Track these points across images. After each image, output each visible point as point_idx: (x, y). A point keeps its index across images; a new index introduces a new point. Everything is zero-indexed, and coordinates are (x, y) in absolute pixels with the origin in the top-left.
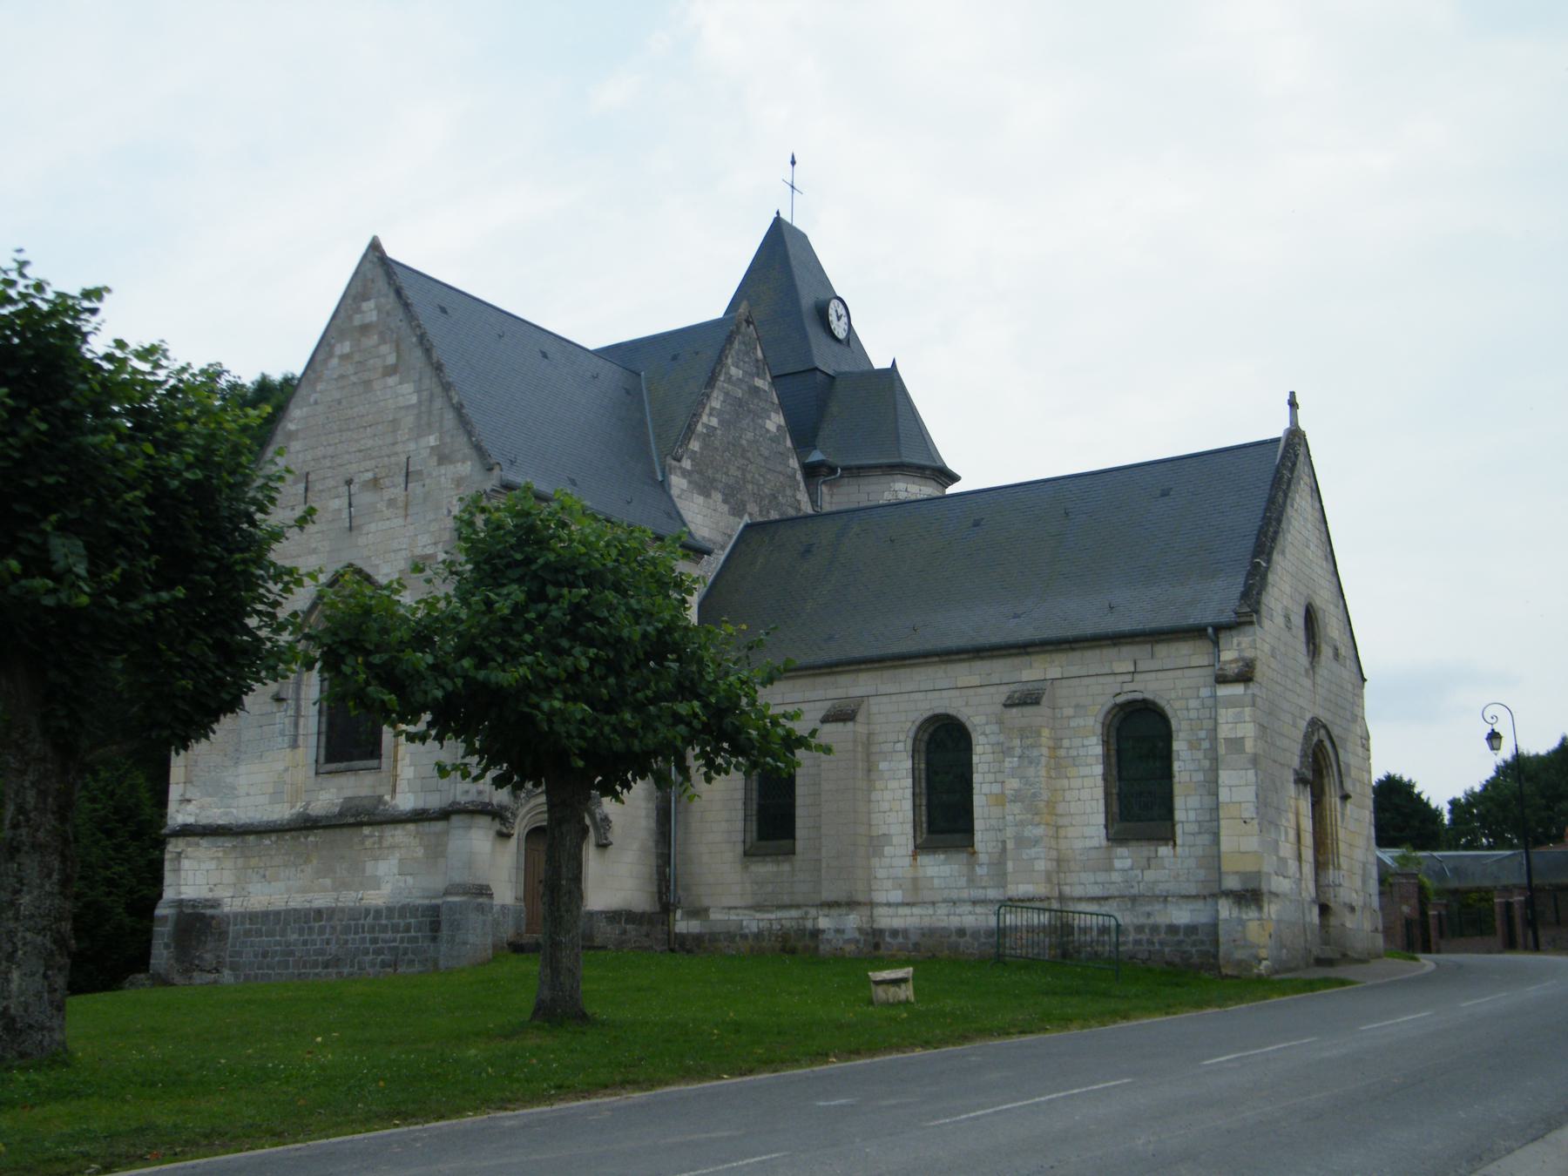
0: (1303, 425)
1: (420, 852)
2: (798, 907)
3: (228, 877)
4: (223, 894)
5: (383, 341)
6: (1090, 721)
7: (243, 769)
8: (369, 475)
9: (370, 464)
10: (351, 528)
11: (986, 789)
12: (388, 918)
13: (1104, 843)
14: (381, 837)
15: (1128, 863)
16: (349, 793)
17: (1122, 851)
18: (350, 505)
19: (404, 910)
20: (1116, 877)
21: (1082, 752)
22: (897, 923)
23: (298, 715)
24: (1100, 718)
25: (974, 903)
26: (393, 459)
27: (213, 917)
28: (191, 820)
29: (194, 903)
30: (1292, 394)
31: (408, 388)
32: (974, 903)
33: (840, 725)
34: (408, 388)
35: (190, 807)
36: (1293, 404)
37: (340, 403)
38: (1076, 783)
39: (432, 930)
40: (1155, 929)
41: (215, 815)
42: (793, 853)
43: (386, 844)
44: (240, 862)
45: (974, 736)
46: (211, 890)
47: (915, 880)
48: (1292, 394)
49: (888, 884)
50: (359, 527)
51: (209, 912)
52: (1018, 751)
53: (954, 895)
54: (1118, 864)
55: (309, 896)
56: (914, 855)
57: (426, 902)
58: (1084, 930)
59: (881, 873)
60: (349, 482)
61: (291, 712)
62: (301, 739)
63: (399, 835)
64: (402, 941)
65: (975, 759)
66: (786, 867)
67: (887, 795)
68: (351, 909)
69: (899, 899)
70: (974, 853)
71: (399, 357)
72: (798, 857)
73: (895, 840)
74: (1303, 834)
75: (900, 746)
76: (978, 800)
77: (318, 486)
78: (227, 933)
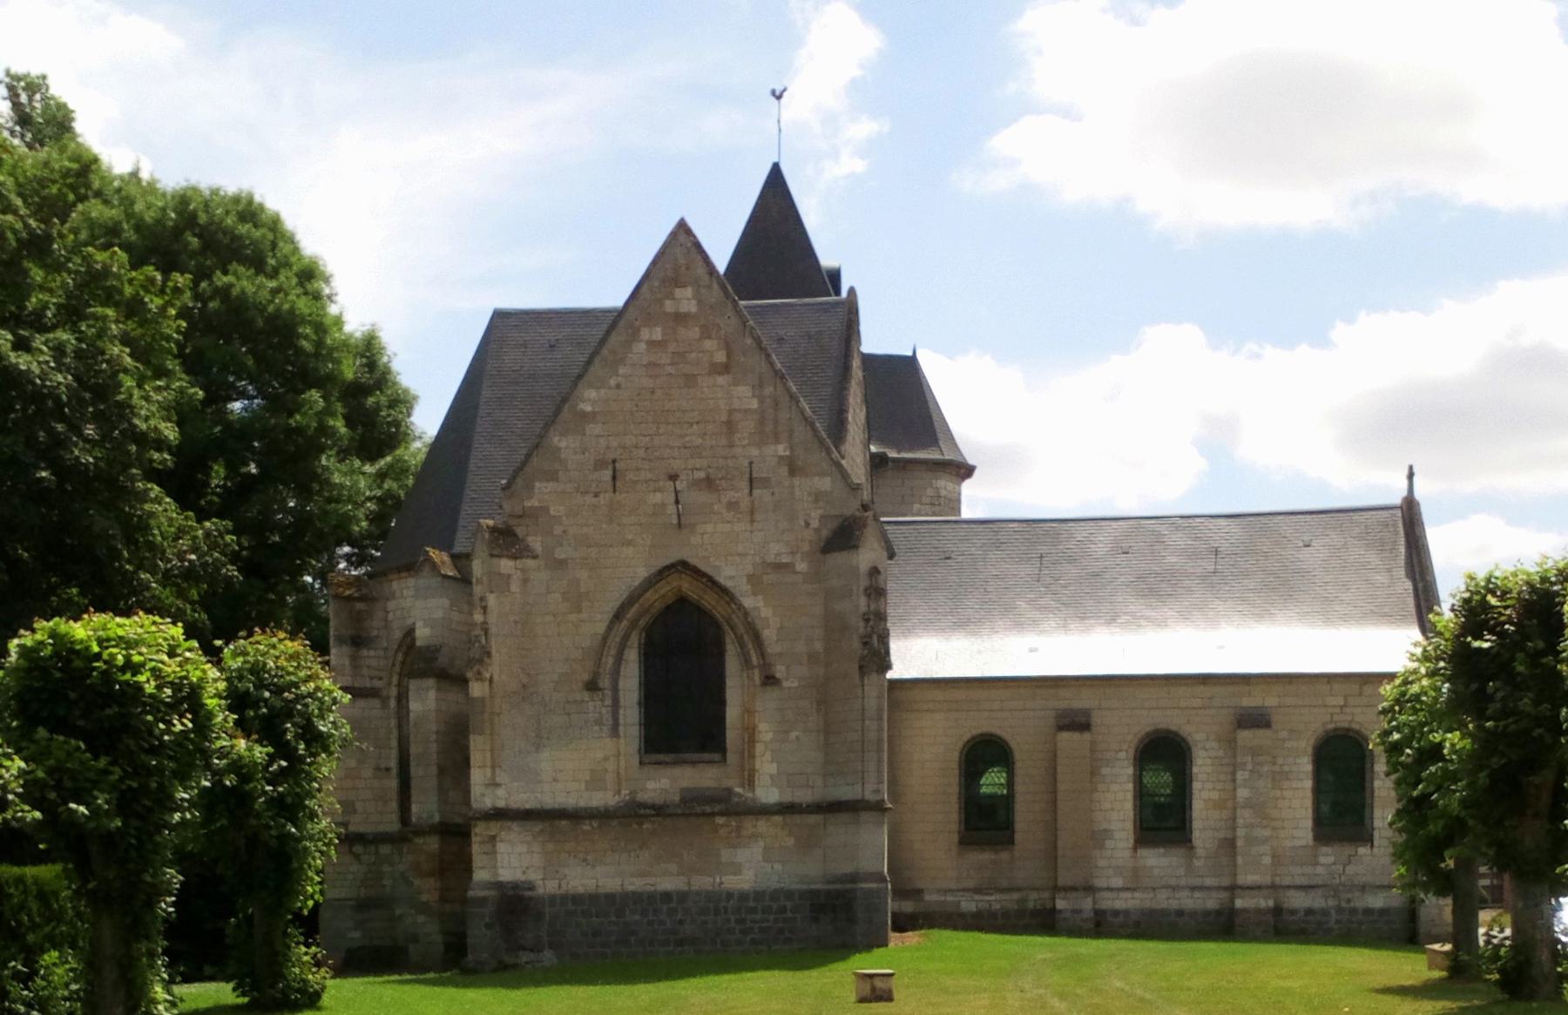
0: (1419, 494)
1: (791, 842)
2: (1019, 890)
3: (537, 860)
4: (534, 876)
5: (706, 333)
6: (1303, 744)
7: (545, 754)
8: (702, 475)
9: (698, 463)
10: (679, 525)
11: (1205, 795)
12: (755, 900)
13: (1311, 843)
14: (739, 829)
15: (1331, 859)
16: (685, 784)
17: (1325, 849)
18: (677, 502)
19: (789, 894)
20: (1320, 870)
21: (1294, 768)
22: (1119, 904)
24: (1312, 742)
25: (1193, 889)
26: (730, 462)
27: (531, 898)
28: (501, 804)
29: (516, 886)
30: (1411, 468)
31: (743, 391)
32: (1193, 889)
34: (743, 391)
35: (500, 792)
36: (1411, 476)
38: (1287, 793)
40: (1354, 911)
41: (522, 799)
43: (744, 833)
44: (550, 847)
45: (1194, 750)
48: (1411, 468)
50: (693, 526)
51: (529, 893)
52: (1249, 767)
53: (1173, 882)
54: (1322, 860)
55: (651, 880)
56: (1135, 849)
57: (805, 887)
58: (1293, 912)
59: (1102, 863)
60: (673, 477)
61: (608, 702)
62: (621, 729)
63: (762, 825)
64: (776, 921)
65: (1195, 770)
66: (1004, 856)
70: (1192, 848)
71: (729, 356)
73: (1117, 835)
75: (1122, 755)
77: (630, 476)
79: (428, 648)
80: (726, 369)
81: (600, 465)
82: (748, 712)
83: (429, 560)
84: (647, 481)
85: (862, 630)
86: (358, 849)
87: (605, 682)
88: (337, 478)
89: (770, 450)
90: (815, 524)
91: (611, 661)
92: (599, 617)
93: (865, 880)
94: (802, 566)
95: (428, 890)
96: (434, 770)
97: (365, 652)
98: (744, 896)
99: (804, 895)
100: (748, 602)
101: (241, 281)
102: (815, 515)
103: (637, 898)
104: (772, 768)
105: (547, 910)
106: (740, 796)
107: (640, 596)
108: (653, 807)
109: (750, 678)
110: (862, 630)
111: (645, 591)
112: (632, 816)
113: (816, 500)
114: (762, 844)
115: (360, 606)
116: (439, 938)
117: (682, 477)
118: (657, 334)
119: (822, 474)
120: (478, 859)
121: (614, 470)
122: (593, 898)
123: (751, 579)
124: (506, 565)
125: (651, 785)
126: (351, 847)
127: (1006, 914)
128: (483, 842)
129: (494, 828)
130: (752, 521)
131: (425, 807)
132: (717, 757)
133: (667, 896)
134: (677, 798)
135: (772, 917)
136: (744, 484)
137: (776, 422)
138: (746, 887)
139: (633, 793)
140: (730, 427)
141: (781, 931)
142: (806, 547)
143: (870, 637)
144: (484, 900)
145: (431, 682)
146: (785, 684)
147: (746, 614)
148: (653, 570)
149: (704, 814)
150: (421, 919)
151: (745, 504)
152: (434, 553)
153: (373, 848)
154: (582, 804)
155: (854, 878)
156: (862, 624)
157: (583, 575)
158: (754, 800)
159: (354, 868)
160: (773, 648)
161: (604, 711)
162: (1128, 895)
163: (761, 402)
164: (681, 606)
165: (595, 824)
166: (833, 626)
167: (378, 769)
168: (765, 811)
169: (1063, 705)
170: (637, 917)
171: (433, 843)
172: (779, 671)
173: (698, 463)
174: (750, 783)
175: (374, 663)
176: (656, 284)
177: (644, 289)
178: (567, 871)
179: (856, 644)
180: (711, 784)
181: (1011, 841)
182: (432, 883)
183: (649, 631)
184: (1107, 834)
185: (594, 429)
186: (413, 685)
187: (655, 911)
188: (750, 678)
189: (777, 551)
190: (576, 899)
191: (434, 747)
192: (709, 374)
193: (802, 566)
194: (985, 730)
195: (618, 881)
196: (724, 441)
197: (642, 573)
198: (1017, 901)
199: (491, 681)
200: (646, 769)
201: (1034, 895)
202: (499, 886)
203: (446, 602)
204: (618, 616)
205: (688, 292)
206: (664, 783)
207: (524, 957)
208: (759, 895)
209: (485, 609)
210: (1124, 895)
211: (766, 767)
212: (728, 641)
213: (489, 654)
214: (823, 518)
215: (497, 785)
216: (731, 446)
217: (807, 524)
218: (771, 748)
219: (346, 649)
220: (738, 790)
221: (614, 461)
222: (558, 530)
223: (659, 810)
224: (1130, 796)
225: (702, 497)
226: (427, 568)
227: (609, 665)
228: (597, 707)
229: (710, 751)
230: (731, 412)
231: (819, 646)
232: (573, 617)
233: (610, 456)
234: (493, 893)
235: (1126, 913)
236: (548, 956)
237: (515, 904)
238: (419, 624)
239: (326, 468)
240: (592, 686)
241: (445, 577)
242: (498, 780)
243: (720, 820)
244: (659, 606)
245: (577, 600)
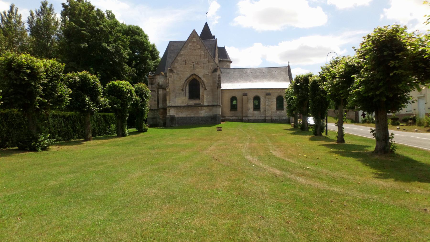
0: (290, 65)
3: (175, 112)
4: (175, 115)
5: (197, 44)
7: (176, 99)
19: (208, 117)
29: (172, 116)
31: (202, 52)
34: (202, 52)
39: (240, 119)
60: (193, 63)
63: (205, 108)
74: (160, 101)
76: (261, 105)
80: (200, 49)
81: (183, 61)
82: (203, 93)
87: (184, 89)
94: (210, 74)
95: (161, 116)
98: (202, 117)
99: (210, 117)
100: (203, 79)
101: (137, 37)
102: (211, 68)
103: (188, 117)
112: (187, 107)
120: (168, 112)
122: (183, 117)
124: (171, 74)
129: (170, 108)
131: (161, 106)
133: (192, 117)
140: (200, 56)
144: (168, 118)
155: (216, 115)
166: (214, 82)
168: (205, 106)
171: (162, 110)
172: (207, 88)
174: (203, 103)
179: (217, 84)
181: (237, 110)
182: (162, 115)
183: (190, 83)
184: (249, 109)
185: (183, 56)
186: (159, 90)
189: (206, 72)
190: (180, 117)
193: (210, 74)
197: (189, 75)
202: (170, 116)
204: (186, 81)
207: (174, 125)
208: (204, 117)
211: (205, 100)
218: (206, 98)
228: (183, 93)
237: (172, 118)
240: (182, 90)
245: (180, 79)
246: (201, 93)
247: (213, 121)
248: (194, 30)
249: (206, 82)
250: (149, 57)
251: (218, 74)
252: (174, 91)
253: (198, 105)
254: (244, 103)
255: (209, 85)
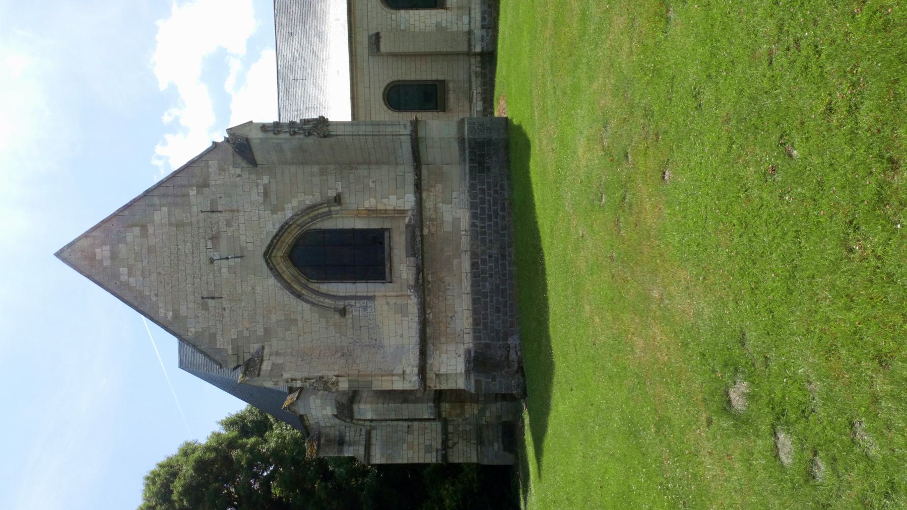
1: (439, 187)
2: (470, 77)
3: (451, 347)
4: (462, 349)
5: (122, 240)
8: (209, 243)
9: (202, 245)
12: (476, 209)
14: (431, 220)
16: (403, 253)
18: (227, 258)
19: (472, 187)
23: (355, 298)
26: (201, 225)
27: (476, 352)
28: (416, 370)
29: (468, 362)
31: (157, 216)
33: (381, 40)
34: (157, 216)
35: (408, 371)
37: (160, 273)
39: (483, 65)
41: (413, 357)
42: (444, 81)
44: (443, 339)
46: (459, 356)
47: (458, 8)
49: (460, 23)
50: (242, 249)
51: (473, 354)
55: (464, 275)
56: (446, 9)
60: (212, 261)
61: (353, 302)
62: (369, 294)
63: (428, 205)
64: (489, 195)
66: (451, 85)
67: (417, 24)
68: (471, 239)
69: (467, 17)
71: (137, 226)
72: (446, 78)
73: (439, 20)
75: (394, 17)
77: (212, 288)
78: (485, 344)
79: (337, 408)
80: (144, 227)
81: (206, 308)
82: (358, 214)
83: (289, 407)
84: (215, 277)
85: (301, 136)
86: (450, 443)
87: (341, 304)
88: (273, 445)
89: (193, 200)
90: (238, 171)
91: (327, 301)
92: (299, 308)
93: (463, 134)
94: (266, 179)
95: (472, 410)
96: (405, 406)
97: (347, 438)
98: (474, 216)
99: (472, 178)
100: (289, 214)
101: (178, 486)
102: (232, 170)
103: (475, 284)
104: (393, 198)
105: (483, 342)
106: (410, 219)
107: (286, 281)
108: (418, 274)
109: (337, 212)
110: (301, 136)
111: (283, 278)
112: (423, 287)
113: (224, 170)
114: (440, 205)
115: (322, 441)
116: (499, 404)
117: (211, 255)
118: (124, 270)
119: (208, 166)
120: (451, 385)
121: (208, 298)
122: (475, 312)
123: (274, 211)
124: (266, 366)
125: (404, 276)
126: (448, 447)
127: (484, 84)
128: (440, 383)
129: (430, 375)
130: (238, 211)
131: (425, 410)
132: (387, 234)
133: (474, 265)
134: (413, 259)
135: (487, 198)
136: (215, 216)
137: (176, 196)
138: (468, 214)
139: (409, 287)
140: (179, 225)
141: (496, 192)
142: (253, 177)
143: (304, 130)
144: (477, 382)
145: (355, 407)
146: (340, 190)
147: (297, 215)
148: (270, 273)
149: (422, 241)
150: (488, 414)
151: (228, 215)
152: (286, 404)
153: (450, 436)
154: (416, 319)
155: (461, 140)
156: (297, 136)
157: (274, 317)
158: (413, 210)
159: (460, 446)
160: (317, 198)
161: (358, 305)
162: (473, 11)
163: (164, 205)
164: (293, 256)
165: (429, 311)
166: (303, 158)
167: (408, 432)
168: (420, 203)
169: (366, 51)
170: (487, 284)
171: (446, 406)
172: (332, 194)
173: (202, 245)
174: (403, 212)
175: (353, 433)
176: (93, 270)
177: (96, 278)
178: (458, 329)
179: (310, 140)
180: (403, 237)
181: (443, 82)
182: (467, 407)
183: (309, 277)
184: (438, 25)
185: (183, 311)
186: (357, 416)
187: (483, 273)
188: (337, 212)
189: (256, 195)
190: (476, 323)
191: (392, 405)
192: (147, 237)
193: (266, 179)
194: (381, 97)
195: (464, 296)
196: (188, 229)
197: (272, 281)
198: (477, 77)
199: (337, 376)
200: (394, 279)
201: (473, 68)
202: (468, 372)
203: (312, 398)
204: (299, 296)
205: (98, 251)
206: (403, 267)
207: (513, 356)
208: (473, 206)
209: (293, 380)
210: (473, 15)
211: (392, 202)
212: (314, 227)
213: (321, 377)
214: (235, 165)
215: (404, 372)
216: (191, 224)
217: (239, 176)
218: (378, 199)
219: (345, 448)
220: (407, 220)
221: (203, 298)
222: (246, 334)
223: (420, 270)
224: (417, 12)
225: (223, 244)
226: (294, 408)
227: (330, 302)
228: (356, 309)
229: (383, 238)
230: (170, 224)
231: (316, 169)
232: (300, 324)
233: (200, 301)
234: (472, 376)
235: (483, 13)
236: (513, 341)
237: (478, 362)
238: (324, 412)
239: (268, 450)
240: (343, 312)
241: (298, 398)
242: (401, 372)
243: (426, 231)
244: (294, 271)
245: (289, 322)
246: (360, 224)
247: (497, 156)
248: (58, 254)
249: (301, 197)
250: (254, 445)
251: (261, 135)
252: (346, 354)
253: (413, 236)
254: (411, 50)
255: (316, 180)
